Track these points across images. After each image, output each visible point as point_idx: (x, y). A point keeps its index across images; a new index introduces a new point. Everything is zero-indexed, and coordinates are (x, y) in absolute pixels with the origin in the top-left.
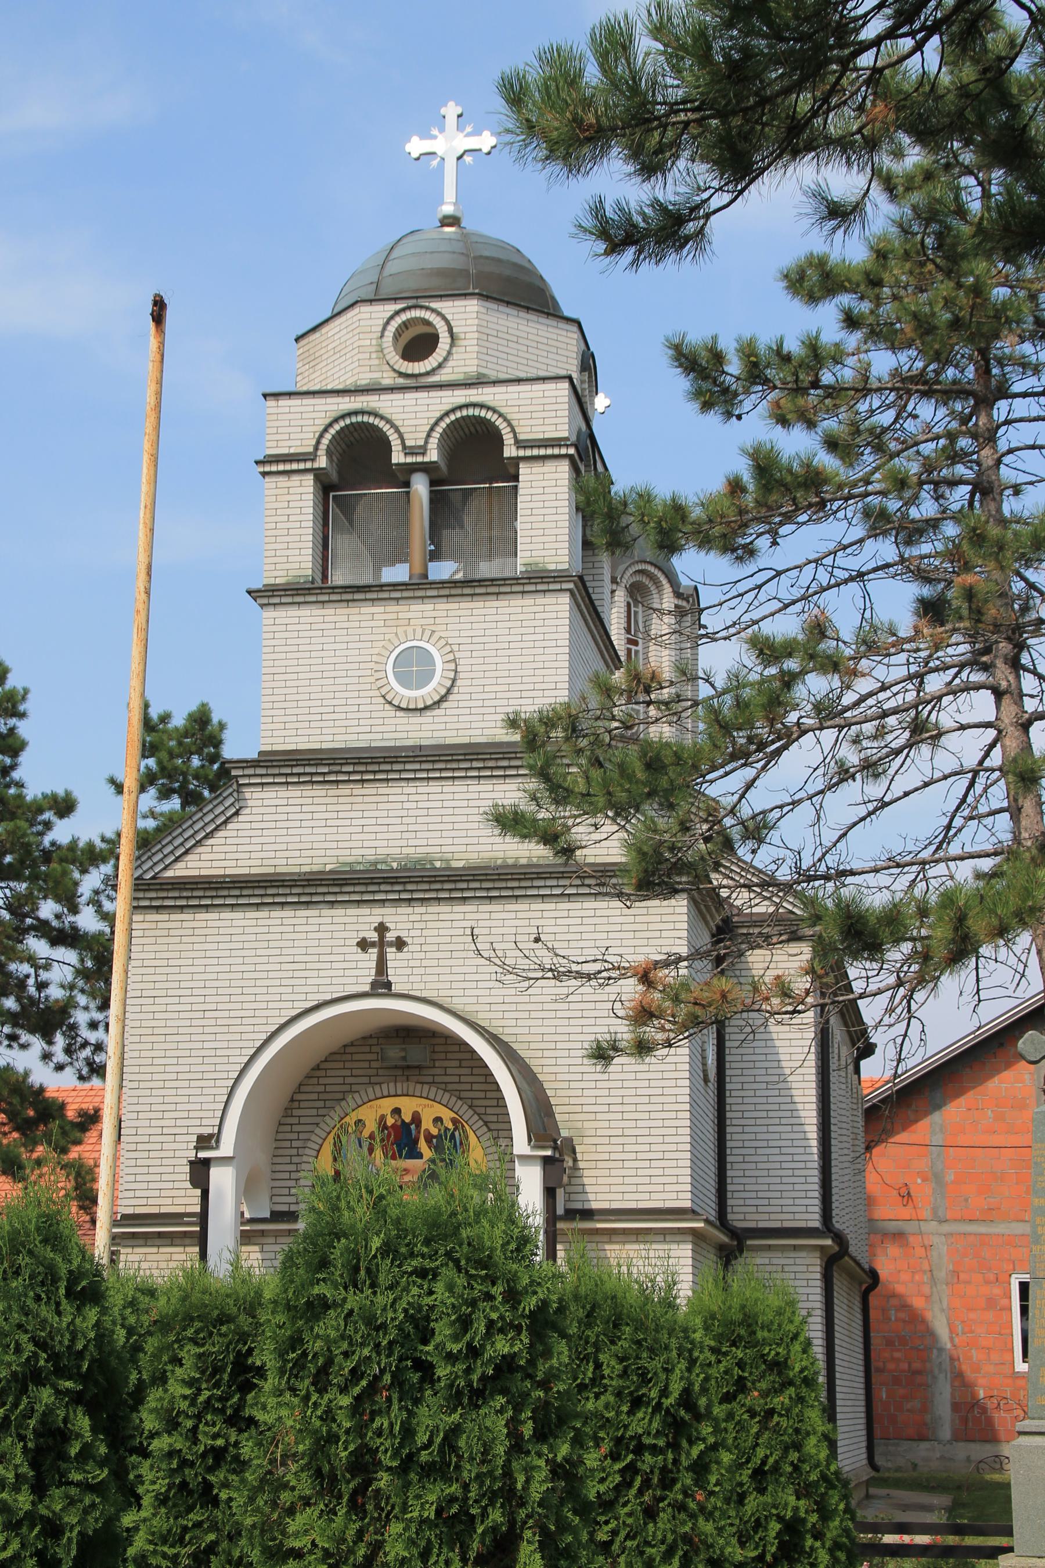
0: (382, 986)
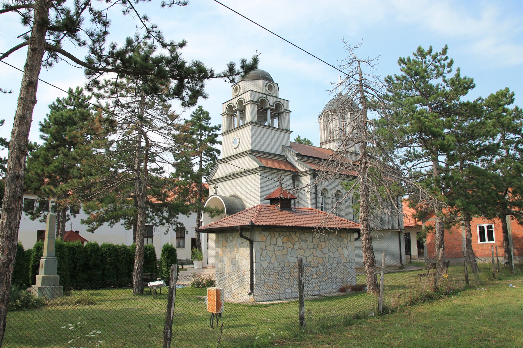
0: (216, 194)
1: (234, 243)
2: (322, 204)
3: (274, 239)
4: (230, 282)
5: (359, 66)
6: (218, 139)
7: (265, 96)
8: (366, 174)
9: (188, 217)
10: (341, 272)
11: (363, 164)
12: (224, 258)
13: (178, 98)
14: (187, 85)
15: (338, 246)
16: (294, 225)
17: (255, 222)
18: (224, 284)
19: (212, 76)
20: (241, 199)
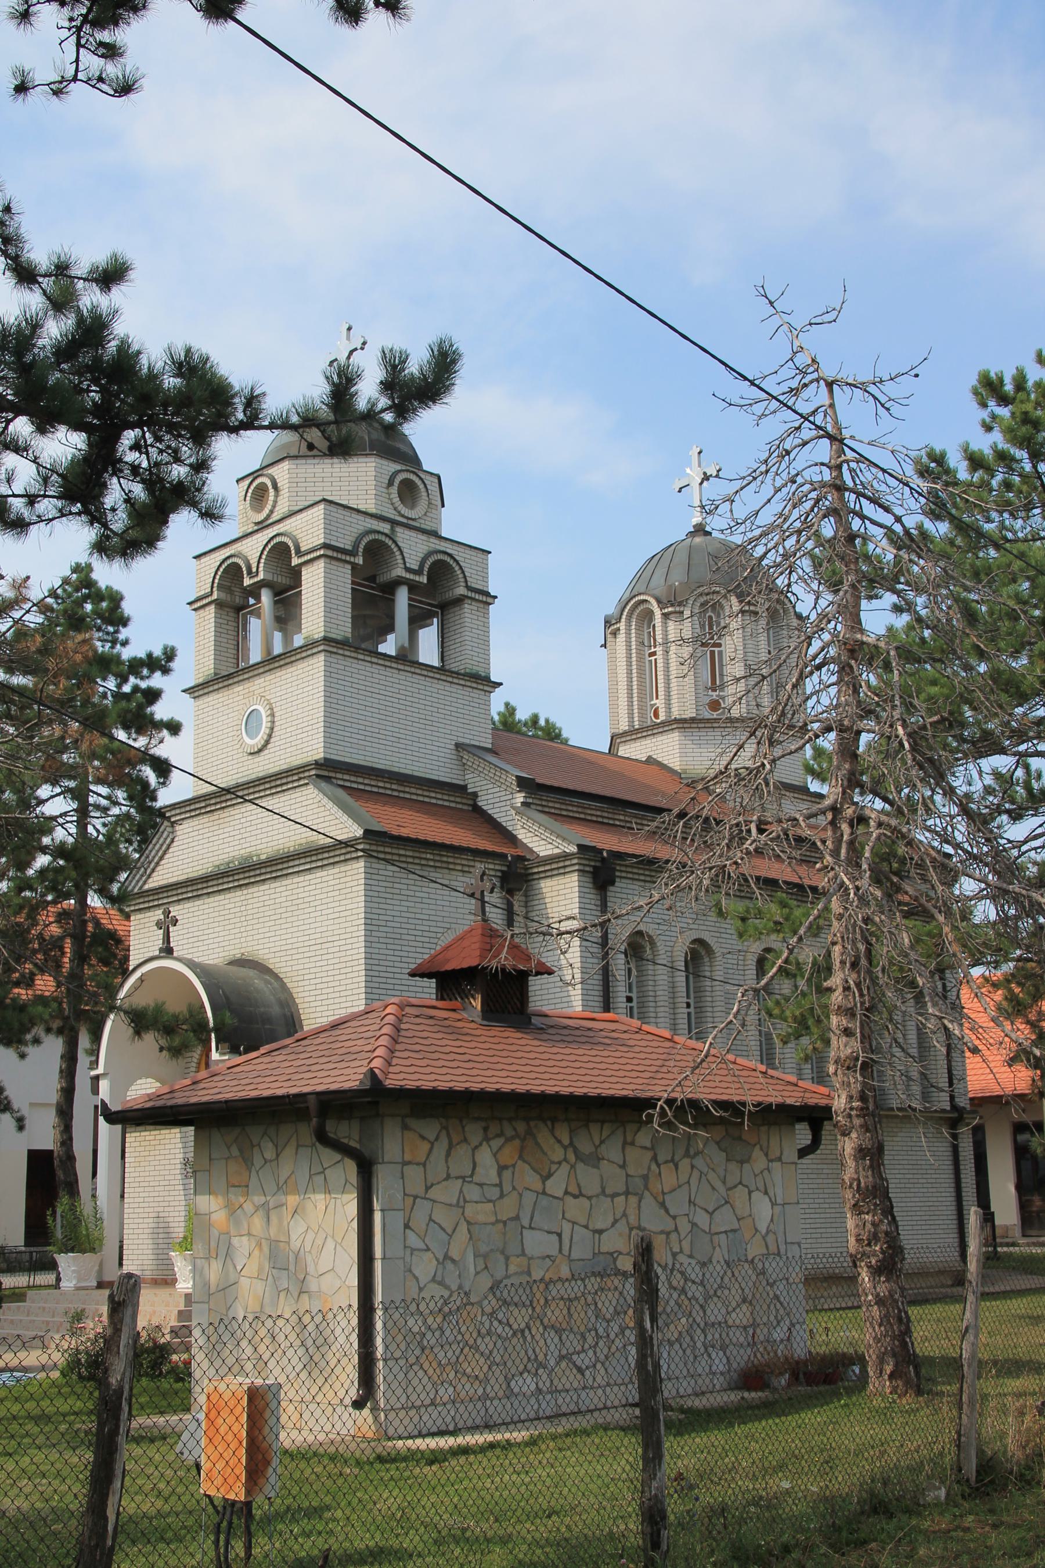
0: (167, 951)
1: (284, 1173)
2: (629, 999)
3: (462, 1152)
4: (262, 1348)
5: (832, 406)
6: (161, 711)
7: (385, 527)
8: (865, 866)
9: (23, 1056)
10: (744, 1301)
11: (845, 828)
12: (235, 1241)
13: (84, 518)
14: (131, 457)
15: (731, 1181)
16: (551, 1087)
17: (386, 1074)
18: (231, 1361)
19: (251, 423)
20: (276, 977)
